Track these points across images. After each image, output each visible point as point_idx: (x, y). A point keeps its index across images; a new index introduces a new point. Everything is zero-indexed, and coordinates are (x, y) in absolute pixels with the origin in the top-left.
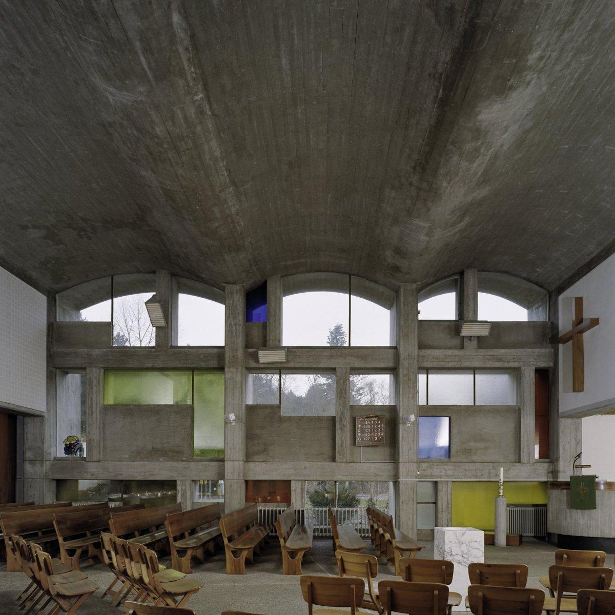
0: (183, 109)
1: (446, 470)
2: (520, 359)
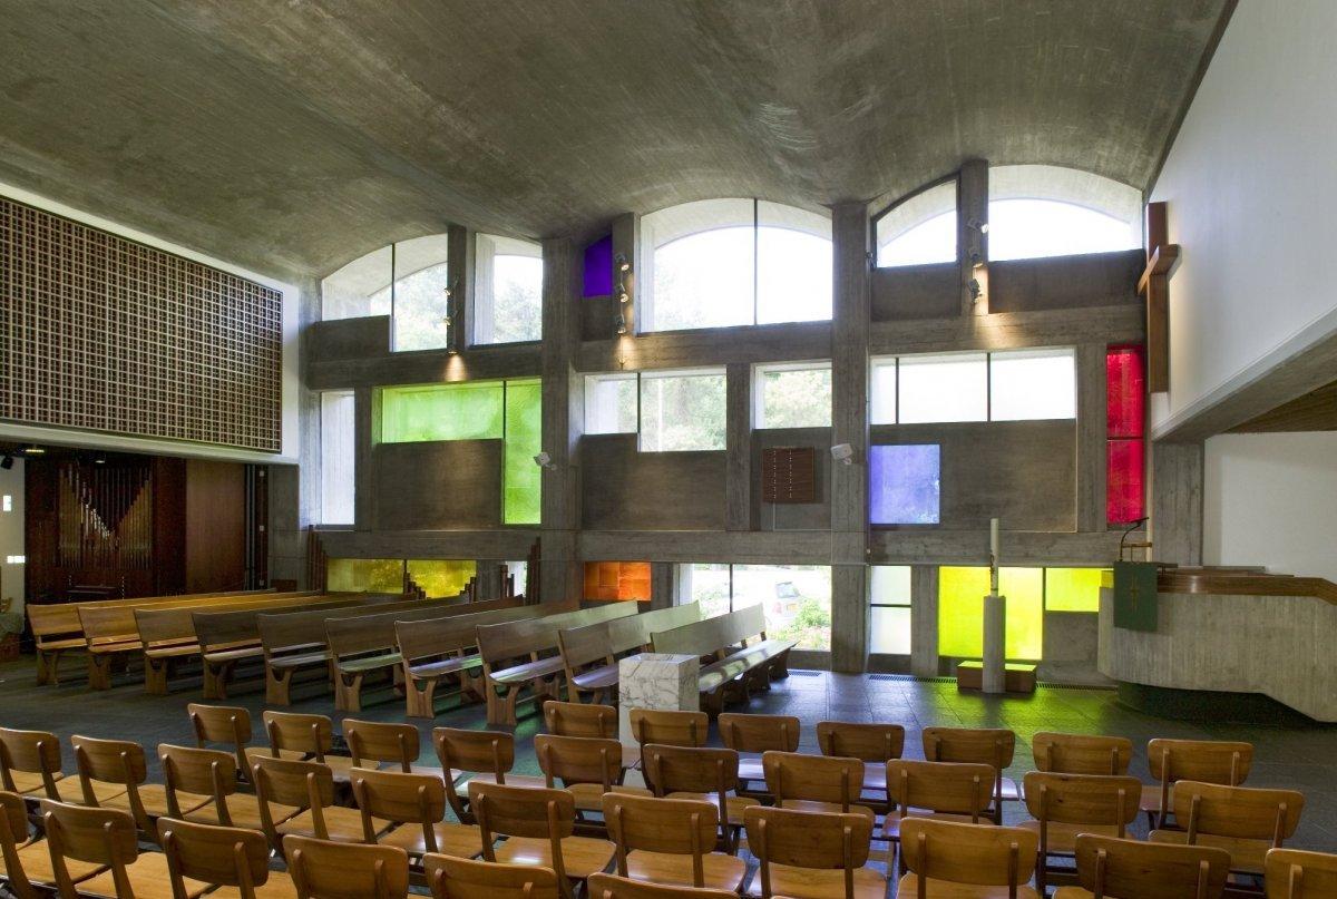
0: (279, 23)
1: (926, 546)
2: (1076, 329)
